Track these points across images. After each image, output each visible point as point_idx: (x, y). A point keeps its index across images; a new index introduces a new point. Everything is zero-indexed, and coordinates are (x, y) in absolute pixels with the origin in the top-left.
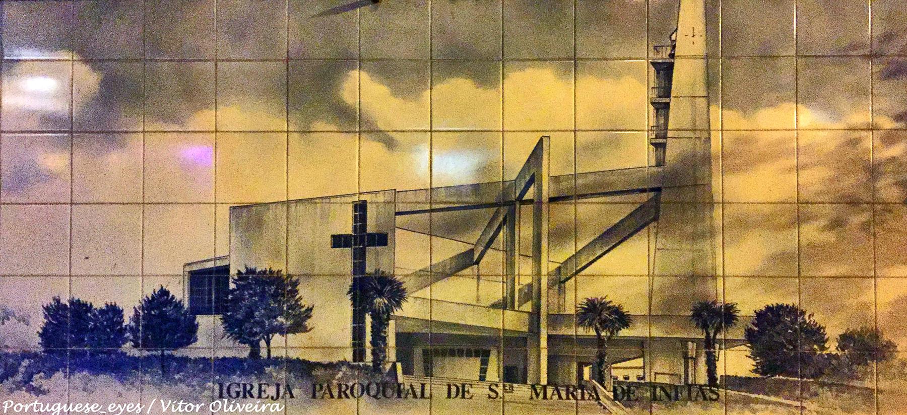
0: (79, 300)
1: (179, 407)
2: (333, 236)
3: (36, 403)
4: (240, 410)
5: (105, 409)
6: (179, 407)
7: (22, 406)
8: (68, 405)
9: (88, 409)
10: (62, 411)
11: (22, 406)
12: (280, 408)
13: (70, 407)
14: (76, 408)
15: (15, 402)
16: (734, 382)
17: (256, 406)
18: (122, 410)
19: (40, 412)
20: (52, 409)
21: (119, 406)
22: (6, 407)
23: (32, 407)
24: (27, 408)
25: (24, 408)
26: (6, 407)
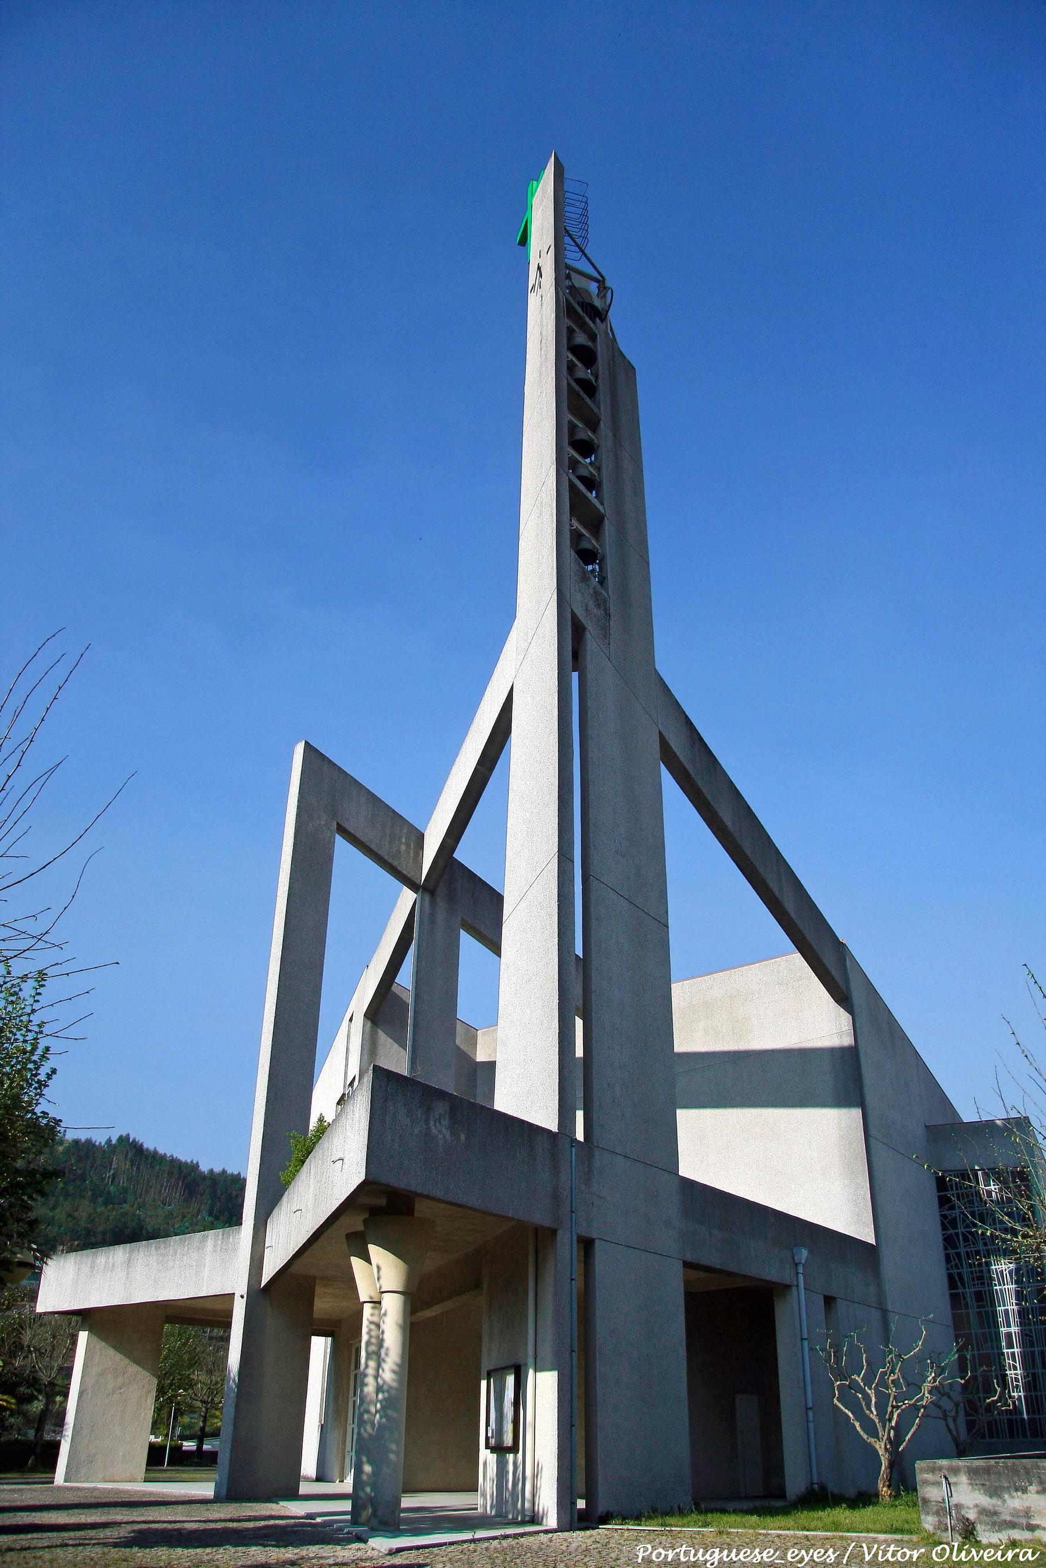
0: (142, 1145)
1: (889, 1555)
2: (495, 1062)
3: (684, 1548)
4: (976, 1559)
5: (783, 1557)
6: (889, 1555)
7: (908, 1553)
8: (730, 1552)
9: (759, 1557)
10: (720, 1560)
11: (908, 1553)
12: (1033, 1554)
13: (733, 1554)
14: (741, 1556)
15: (654, 1548)
16: (574, 1503)
17: (1000, 1553)
18: (807, 1559)
19: (887, 1561)
20: (707, 1556)
21: (803, 1552)
22: (641, 1555)
23: (678, 1555)
24: (671, 1555)
25: (666, 1556)
26: (641, 1555)
